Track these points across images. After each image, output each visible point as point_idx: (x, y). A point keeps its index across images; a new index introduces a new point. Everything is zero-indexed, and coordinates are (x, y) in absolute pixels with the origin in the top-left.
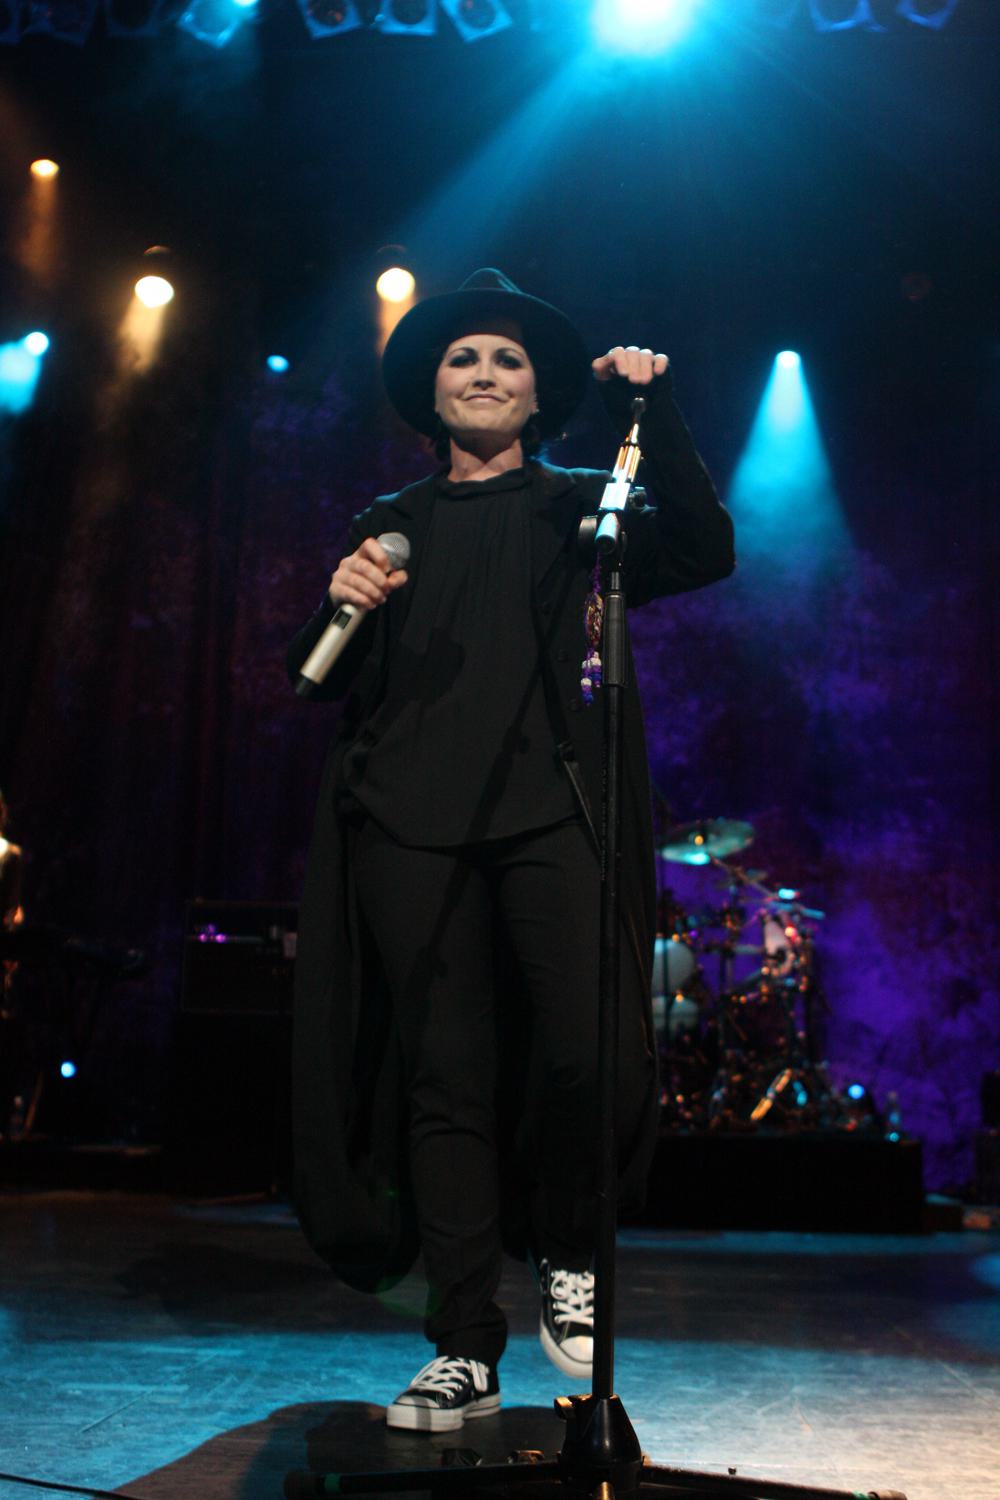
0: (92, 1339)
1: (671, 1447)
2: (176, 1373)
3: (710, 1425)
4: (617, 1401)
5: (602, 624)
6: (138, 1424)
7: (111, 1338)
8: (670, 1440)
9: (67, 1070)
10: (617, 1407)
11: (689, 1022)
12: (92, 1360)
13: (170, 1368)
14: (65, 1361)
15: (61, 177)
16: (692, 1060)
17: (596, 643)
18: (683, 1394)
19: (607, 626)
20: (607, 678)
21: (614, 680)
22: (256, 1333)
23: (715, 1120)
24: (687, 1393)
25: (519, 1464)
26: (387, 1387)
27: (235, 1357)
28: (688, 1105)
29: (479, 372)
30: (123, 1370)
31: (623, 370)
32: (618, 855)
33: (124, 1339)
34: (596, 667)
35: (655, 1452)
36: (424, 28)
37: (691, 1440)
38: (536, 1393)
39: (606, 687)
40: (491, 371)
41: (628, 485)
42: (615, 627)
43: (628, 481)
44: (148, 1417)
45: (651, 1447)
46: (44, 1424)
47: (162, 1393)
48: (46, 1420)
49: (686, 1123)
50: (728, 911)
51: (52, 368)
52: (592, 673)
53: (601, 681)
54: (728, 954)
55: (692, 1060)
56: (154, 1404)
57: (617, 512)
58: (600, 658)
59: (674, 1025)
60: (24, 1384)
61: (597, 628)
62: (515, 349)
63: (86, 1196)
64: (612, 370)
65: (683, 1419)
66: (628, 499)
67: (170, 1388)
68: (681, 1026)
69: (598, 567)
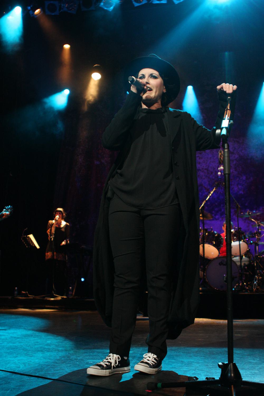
0: (94, 348)
1: (249, 376)
3: (259, 371)
4: (235, 364)
5: (223, 158)
7: (98, 348)
8: (248, 375)
9: (83, 280)
10: (235, 365)
11: (247, 263)
12: (94, 354)
14: (87, 354)
15: (71, 48)
16: (248, 273)
17: (222, 163)
18: (250, 362)
19: (225, 158)
20: (225, 172)
21: (227, 172)
22: (136, 347)
23: (254, 289)
24: (252, 362)
25: (208, 380)
26: (172, 361)
28: (247, 285)
29: (151, 94)
30: (102, 357)
31: (225, 90)
32: (230, 219)
33: (102, 349)
34: (222, 169)
35: (244, 378)
37: (254, 374)
38: (211, 362)
39: (225, 174)
40: (148, 79)
41: (228, 120)
42: (226, 158)
43: (228, 119)
45: (243, 376)
49: (247, 290)
50: (256, 233)
51: (71, 99)
52: (221, 171)
53: (223, 173)
54: (256, 244)
55: (248, 273)
57: (226, 128)
58: (223, 167)
59: (243, 264)
60: (78, 360)
61: (222, 159)
62: (156, 73)
63: (89, 312)
64: (222, 89)
65: (251, 369)
66: (229, 124)
68: (244, 264)
69: (221, 143)
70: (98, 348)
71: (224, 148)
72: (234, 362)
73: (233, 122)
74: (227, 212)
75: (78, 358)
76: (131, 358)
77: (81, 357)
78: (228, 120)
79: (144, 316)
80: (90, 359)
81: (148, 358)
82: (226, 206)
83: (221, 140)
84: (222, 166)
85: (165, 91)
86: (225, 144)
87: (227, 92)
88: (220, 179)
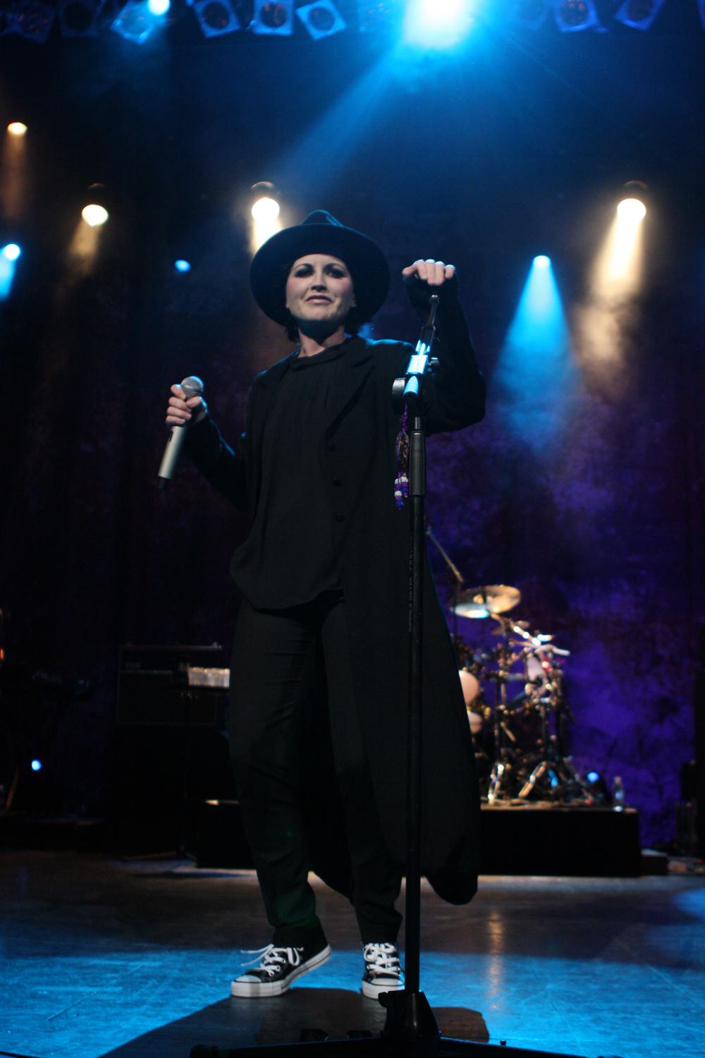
0: (55, 955)
2: (114, 978)
4: (422, 994)
6: (87, 1014)
7: (67, 954)
13: (109, 975)
14: (36, 971)
15: (28, 135)
18: (468, 990)
21: (416, 492)
22: (170, 950)
27: (155, 967)
30: (76, 977)
31: (423, 277)
33: (78, 956)
34: (405, 482)
36: (285, 30)
39: (411, 497)
40: (323, 279)
41: (426, 356)
42: (417, 455)
44: (95, 1009)
46: (21, 1014)
47: (105, 993)
48: (22, 1012)
52: (401, 487)
53: (408, 493)
56: (98, 1000)
57: (418, 376)
58: (407, 477)
62: (338, 264)
64: (416, 275)
67: (110, 989)
69: (405, 413)
70: (67, 954)
71: (411, 429)
72: (420, 991)
73: (437, 362)
74: (413, 595)
75: (7, 980)
76: (154, 980)
77: (16, 980)
78: (426, 356)
79: (199, 866)
80: (40, 984)
81: (380, 961)
82: (413, 579)
83: (406, 407)
84: (405, 474)
85: (354, 305)
86: (416, 418)
87: (431, 281)
88: (400, 509)
